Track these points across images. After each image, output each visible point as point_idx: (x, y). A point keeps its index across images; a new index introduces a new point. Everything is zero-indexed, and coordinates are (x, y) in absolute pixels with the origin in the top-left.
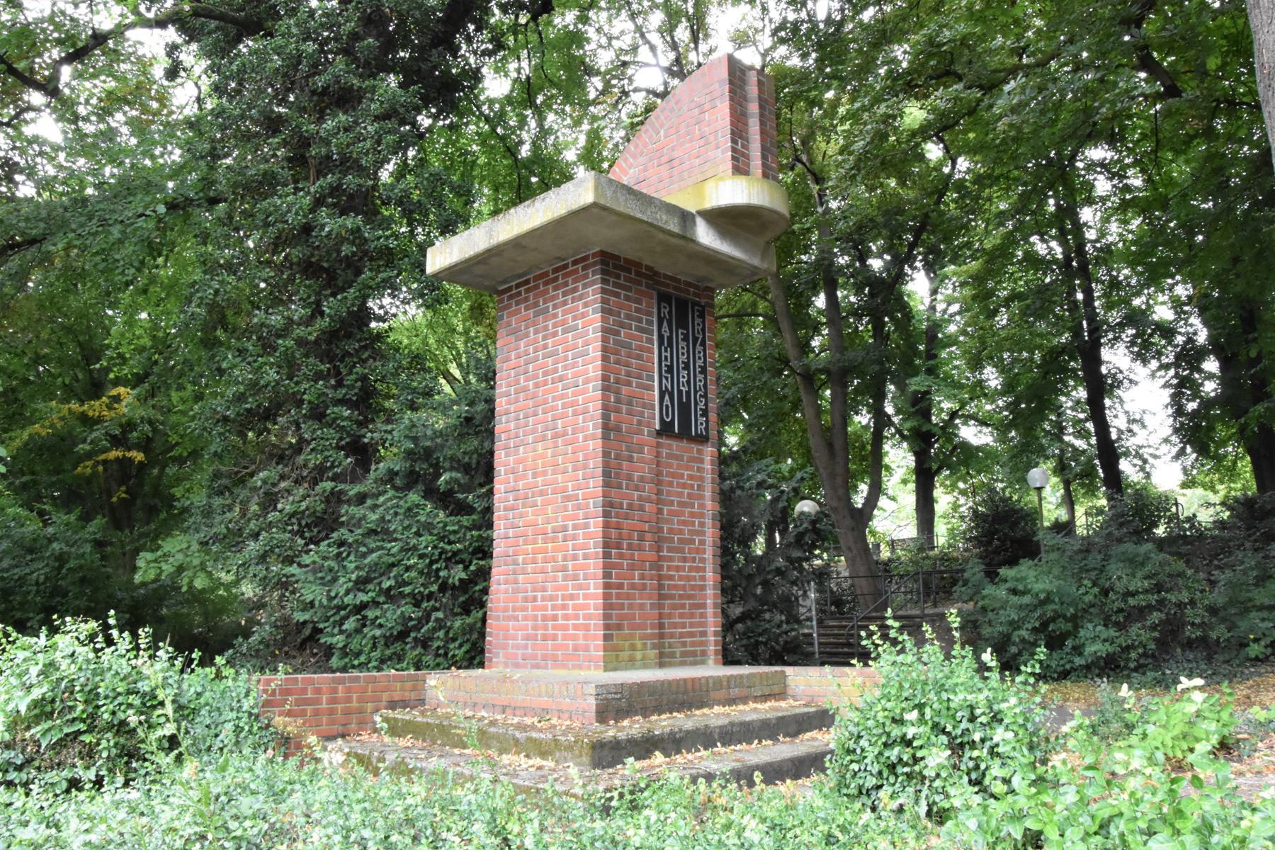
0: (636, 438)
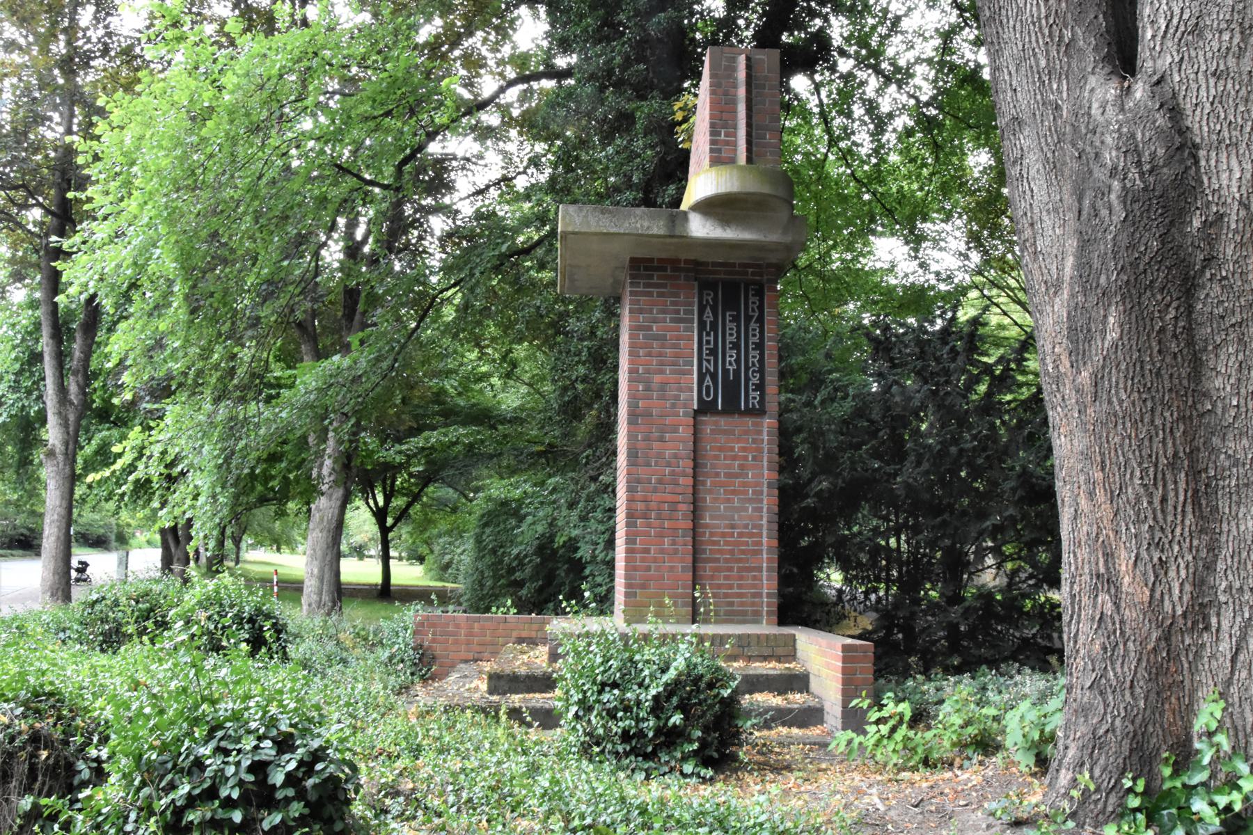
0: (668, 420)
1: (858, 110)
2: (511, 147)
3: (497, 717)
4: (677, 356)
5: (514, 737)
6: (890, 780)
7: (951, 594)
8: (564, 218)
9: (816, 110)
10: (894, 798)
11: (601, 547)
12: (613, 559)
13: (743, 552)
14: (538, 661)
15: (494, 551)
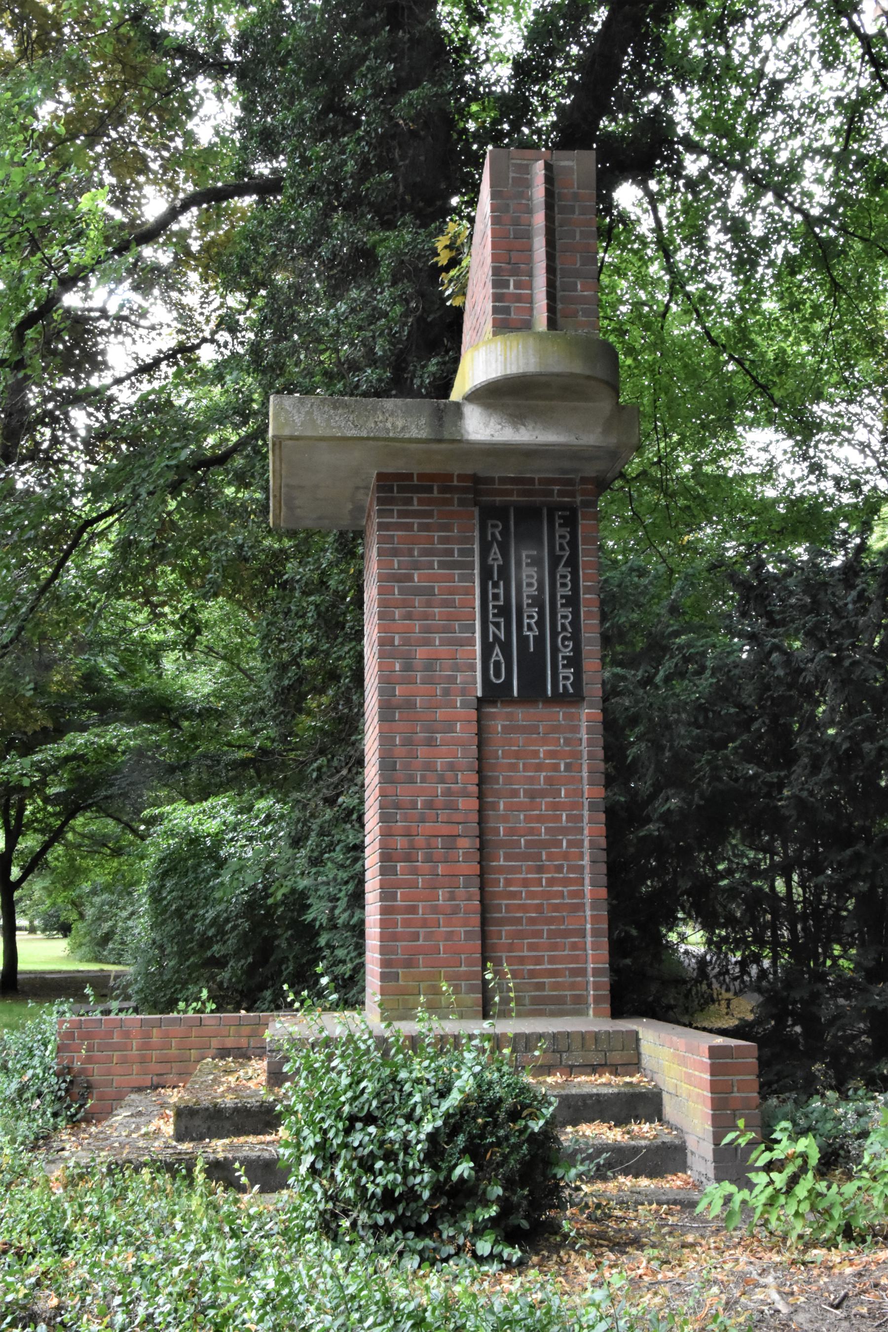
0: (440, 714)
1: (715, 235)
2: (191, 299)
3: (190, 1178)
4: (450, 618)
5: (217, 1208)
6: (793, 1263)
7: (871, 964)
8: (276, 416)
9: (651, 237)
10: (802, 1292)
11: (342, 904)
12: (362, 922)
13: (556, 908)
14: (251, 1084)
15: (179, 914)
